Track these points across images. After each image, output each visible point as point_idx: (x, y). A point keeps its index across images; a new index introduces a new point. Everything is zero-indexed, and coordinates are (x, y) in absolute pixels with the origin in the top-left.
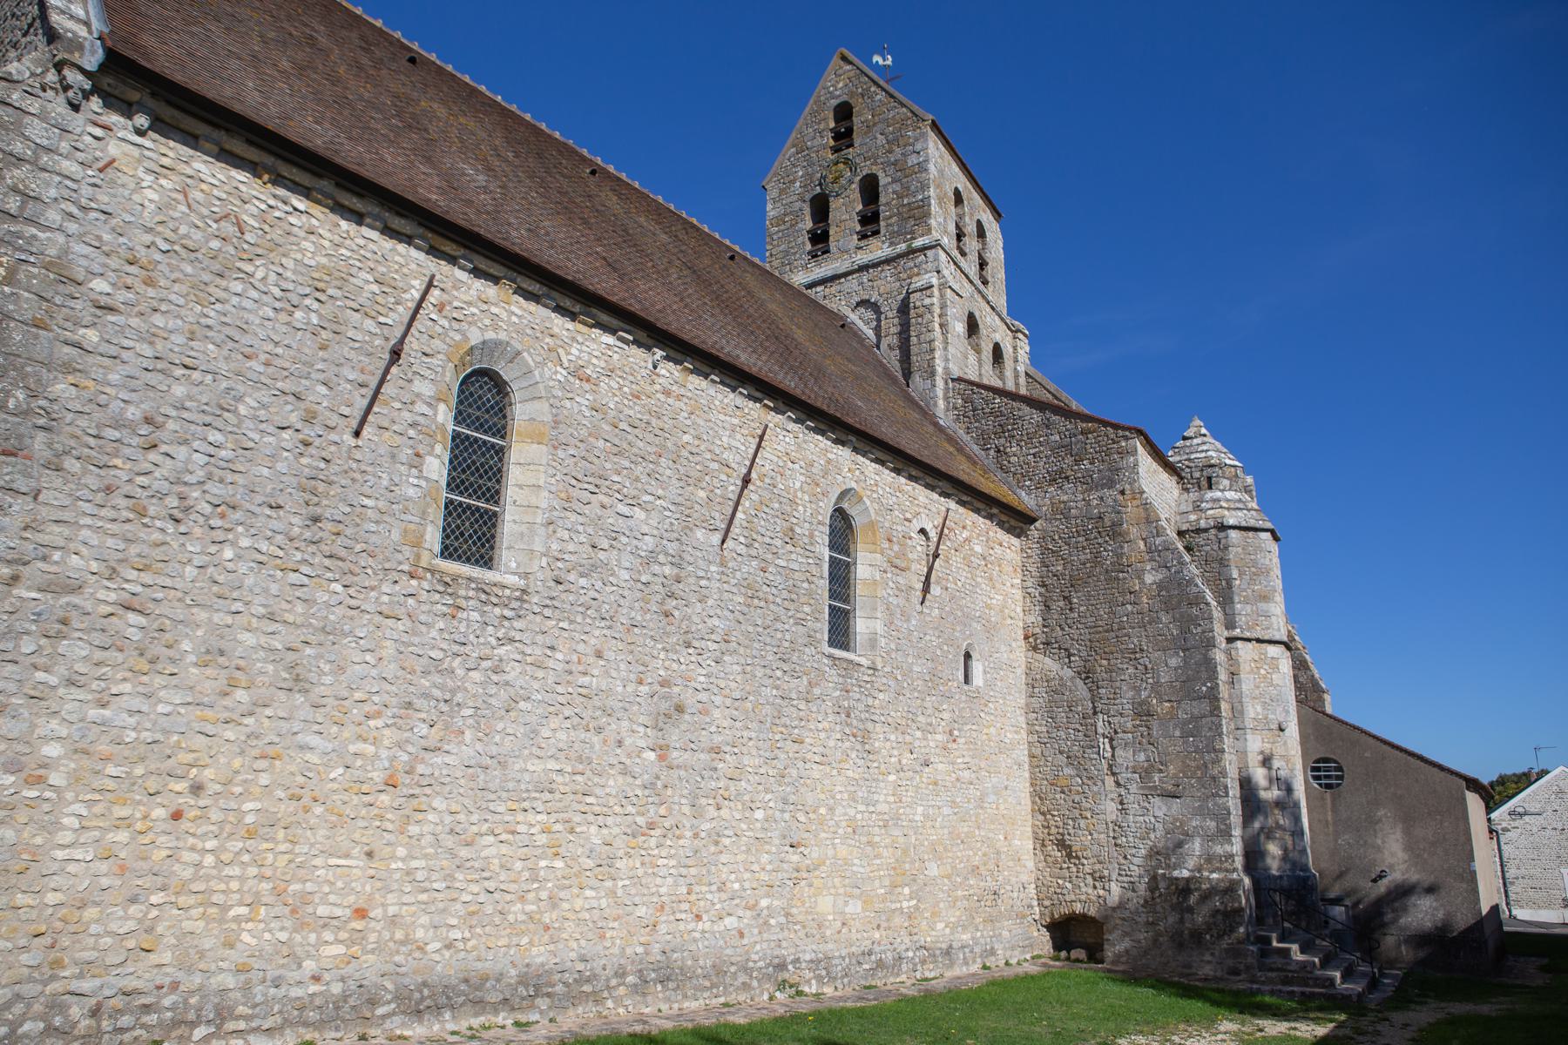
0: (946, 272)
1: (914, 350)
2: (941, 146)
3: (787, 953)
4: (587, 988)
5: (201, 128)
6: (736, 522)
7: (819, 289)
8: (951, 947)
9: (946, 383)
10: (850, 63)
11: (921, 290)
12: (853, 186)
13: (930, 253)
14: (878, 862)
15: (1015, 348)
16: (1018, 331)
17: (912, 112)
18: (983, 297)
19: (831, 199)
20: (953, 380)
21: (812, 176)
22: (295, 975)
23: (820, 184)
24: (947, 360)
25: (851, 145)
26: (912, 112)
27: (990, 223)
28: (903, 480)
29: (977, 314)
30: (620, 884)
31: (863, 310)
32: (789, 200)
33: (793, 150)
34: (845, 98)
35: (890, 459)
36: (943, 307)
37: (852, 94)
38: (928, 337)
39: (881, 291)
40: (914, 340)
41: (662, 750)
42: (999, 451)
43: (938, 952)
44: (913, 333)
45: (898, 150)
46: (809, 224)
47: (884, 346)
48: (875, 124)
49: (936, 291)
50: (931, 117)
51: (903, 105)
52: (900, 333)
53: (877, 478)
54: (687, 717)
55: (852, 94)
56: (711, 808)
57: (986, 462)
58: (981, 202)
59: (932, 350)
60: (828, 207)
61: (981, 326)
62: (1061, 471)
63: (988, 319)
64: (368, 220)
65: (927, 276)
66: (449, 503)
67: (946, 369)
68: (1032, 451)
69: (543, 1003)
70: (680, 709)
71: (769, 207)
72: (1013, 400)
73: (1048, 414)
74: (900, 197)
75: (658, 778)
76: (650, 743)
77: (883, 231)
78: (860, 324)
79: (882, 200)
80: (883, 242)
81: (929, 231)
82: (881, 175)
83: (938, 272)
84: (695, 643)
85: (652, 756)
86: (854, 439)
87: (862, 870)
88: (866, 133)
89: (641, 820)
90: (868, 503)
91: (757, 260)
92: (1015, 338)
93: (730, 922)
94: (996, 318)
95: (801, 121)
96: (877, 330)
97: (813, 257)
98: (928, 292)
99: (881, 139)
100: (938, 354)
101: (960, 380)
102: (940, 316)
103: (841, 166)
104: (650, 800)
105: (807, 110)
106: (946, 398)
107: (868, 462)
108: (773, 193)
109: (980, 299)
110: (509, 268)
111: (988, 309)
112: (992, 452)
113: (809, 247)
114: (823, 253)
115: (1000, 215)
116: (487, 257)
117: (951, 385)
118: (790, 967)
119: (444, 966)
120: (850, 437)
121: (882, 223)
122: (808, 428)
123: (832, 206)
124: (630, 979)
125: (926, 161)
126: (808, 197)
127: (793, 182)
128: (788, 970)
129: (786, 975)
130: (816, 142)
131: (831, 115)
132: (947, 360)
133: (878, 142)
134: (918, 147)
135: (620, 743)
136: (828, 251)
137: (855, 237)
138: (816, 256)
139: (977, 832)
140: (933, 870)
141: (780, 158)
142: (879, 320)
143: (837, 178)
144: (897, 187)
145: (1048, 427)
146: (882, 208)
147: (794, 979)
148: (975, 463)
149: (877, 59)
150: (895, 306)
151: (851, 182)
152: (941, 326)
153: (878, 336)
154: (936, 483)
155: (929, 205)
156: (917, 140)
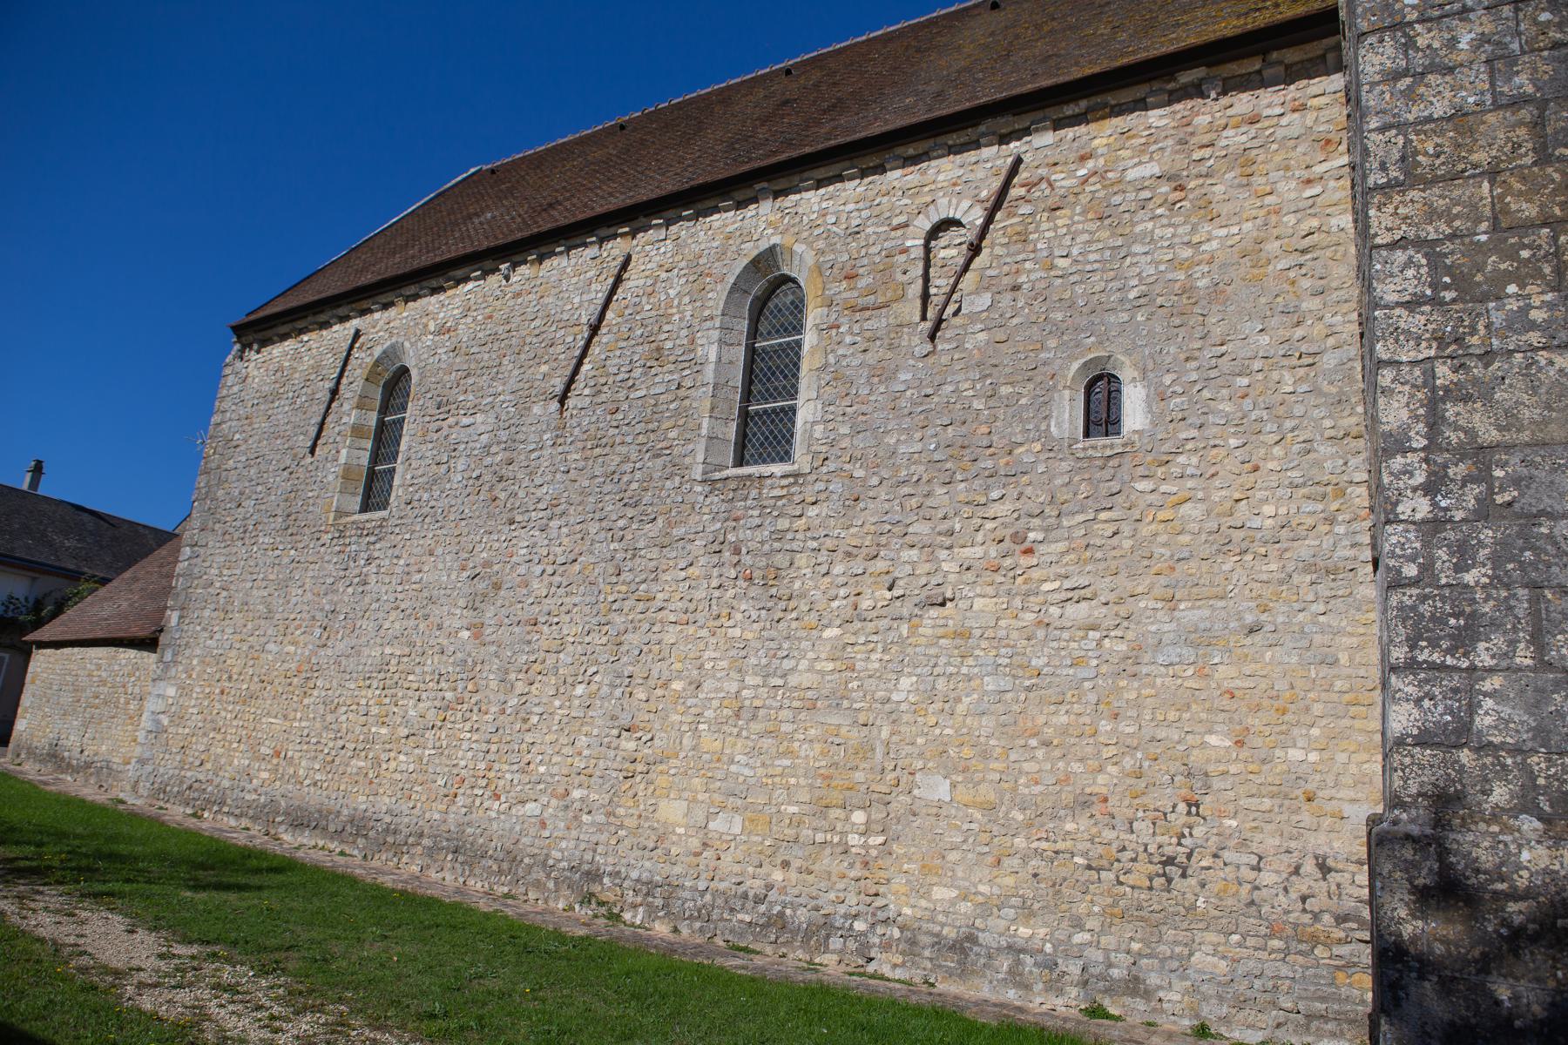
3: (605, 862)
4: (390, 839)
5: (1139, 91)
6: (580, 377)
8: (971, 938)
14: (787, 762)
22: (249, 787)
30: (427, 752)
35: (847, 164)
41: (477, 629)
43: (925, 940)
54: (502, 593)
56: (520, 683)
60: (17, 705)
64: (982, 141)
66: (793, 396)
69: (361, 842)
70: (497, 587)
75: (469, 655)
76: (465, 622)
84: (519, 518)
85: (465, 634)
86: (765, 185)
87: (747, 772)
89: (449, 695)
93: (531, 808)
104: (460, 676)
110: (1150, 80)
116: (381, 293)
118: (606, 880)
119: (314, 798)
120: (757, 187)
122: (688, 219)
124: (426, 842)
128: (601, 883)
129: (596, 888)
135: (440, 627)
139: (1105, 726)
140: (937, 789)
147: (609, 896)
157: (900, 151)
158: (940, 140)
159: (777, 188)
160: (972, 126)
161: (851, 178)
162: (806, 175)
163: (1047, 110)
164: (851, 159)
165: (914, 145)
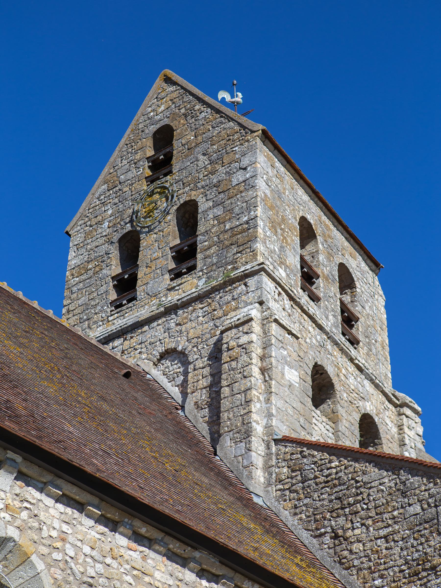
0: (272, 304)
1: (225, 404)
2: (278, 164)
7: (117, 343)
9: (268, 447)
10: (174, 83)
11: (237, 326)
12: (169, 217)
13: (251, 282)
15: (400, 427)
16: (404, 405)
17: (240, 125)
18: (352, 360)
19: (142, 236)
20: (277, 441)
21: (121, 213)
23: (131, 221)
24: (270, 415)
25: (170, 172)
26: (240, 125)
27: (363, 272)
28: (123, 541)
29: (331, 370)
31: (168, 363)
32: (94, 244)
33: (105, 187)
34: (166, 121)
35: (96, 501)
36: (266, 346)
37: (174, 116)
38: (246, 383)
39: (191, 335)
40: (226, 391)
42: (336, 537)
44: (224, 383)
45: (222, 170)
46: (116, 269)
47: (190, 405)
48: (197, 145)
49: (256, 327)
50: (261, 127)
51: (229, 119)
52: (211, 386)
53: (65, 527)
55: (174, 116)
57: (319, 554)
58: (346, 244)
59: (248, 402)
60: (139, 247)
61: (337, 386)
62: (426, 558)
63: (351, 380)
64: (192, 565)
65: (245, 310)
67: (268, 427)
68: (383, 533)
71: (72, 254)
72: (356, 460)
73: (404, 475)
74: (221, 221)
77: (199, 265)
78: (164, 381)
79: (201, 228)
80: (199, 278)
81: (255, 256)
82: (201, 200)
83: (261, 303)
86: (19, 459)
88: (187, 156)
90: (40, 566)
91: (50, 313)
92: (400, 414)
94: (367, 383)
95: (116, 153)
96: (184, 386)
97: (117, 307)
98: (245, 328)
99: (203, 160)
100: (255, 407)
101: (285, 440)
102: (262, 358)
103: (157, 196)
105: (123, 140)
106: (267, 468)
107: (50, 502)
108: (77, 238)
109: (337, 353)
111: (352, 368)
112: (327, 539)
113: (113, 296)
114: (129, 301)
115: (377, 265)
117: (274, 449)
120: (10, 454)
121: (199, 256)
123: (143, 244)
125: (254, 176)
126: (116, 237)
127: (100, 223)
130: (130, 175)
131: (150, 143)
132: (270, 415)
133: (200, 164)
134: (245, 162)
136: (134, 299)
137: (167, 276)
138: (121, 305)
141: (90, 196)
142: (186, 373)
143: (151, 211)
144: (219, 211)
145: (404, 494)
146: (200, 238)
148: (297, 552)
149: (223, 95)
150: (206, 351)
151: (166, 212)
152: (263, 371)
153: (184, 394)
154: (188, 551)
155: (256, 227)
156: (244, 155)
157: (137, 523)
158: (168, 539)
159: (24, 470)
160: (192, 547)
161: (89, 516)
162: (59, 482)
163: (237, 574)
164: (102, 500)
165: (150, 528)
